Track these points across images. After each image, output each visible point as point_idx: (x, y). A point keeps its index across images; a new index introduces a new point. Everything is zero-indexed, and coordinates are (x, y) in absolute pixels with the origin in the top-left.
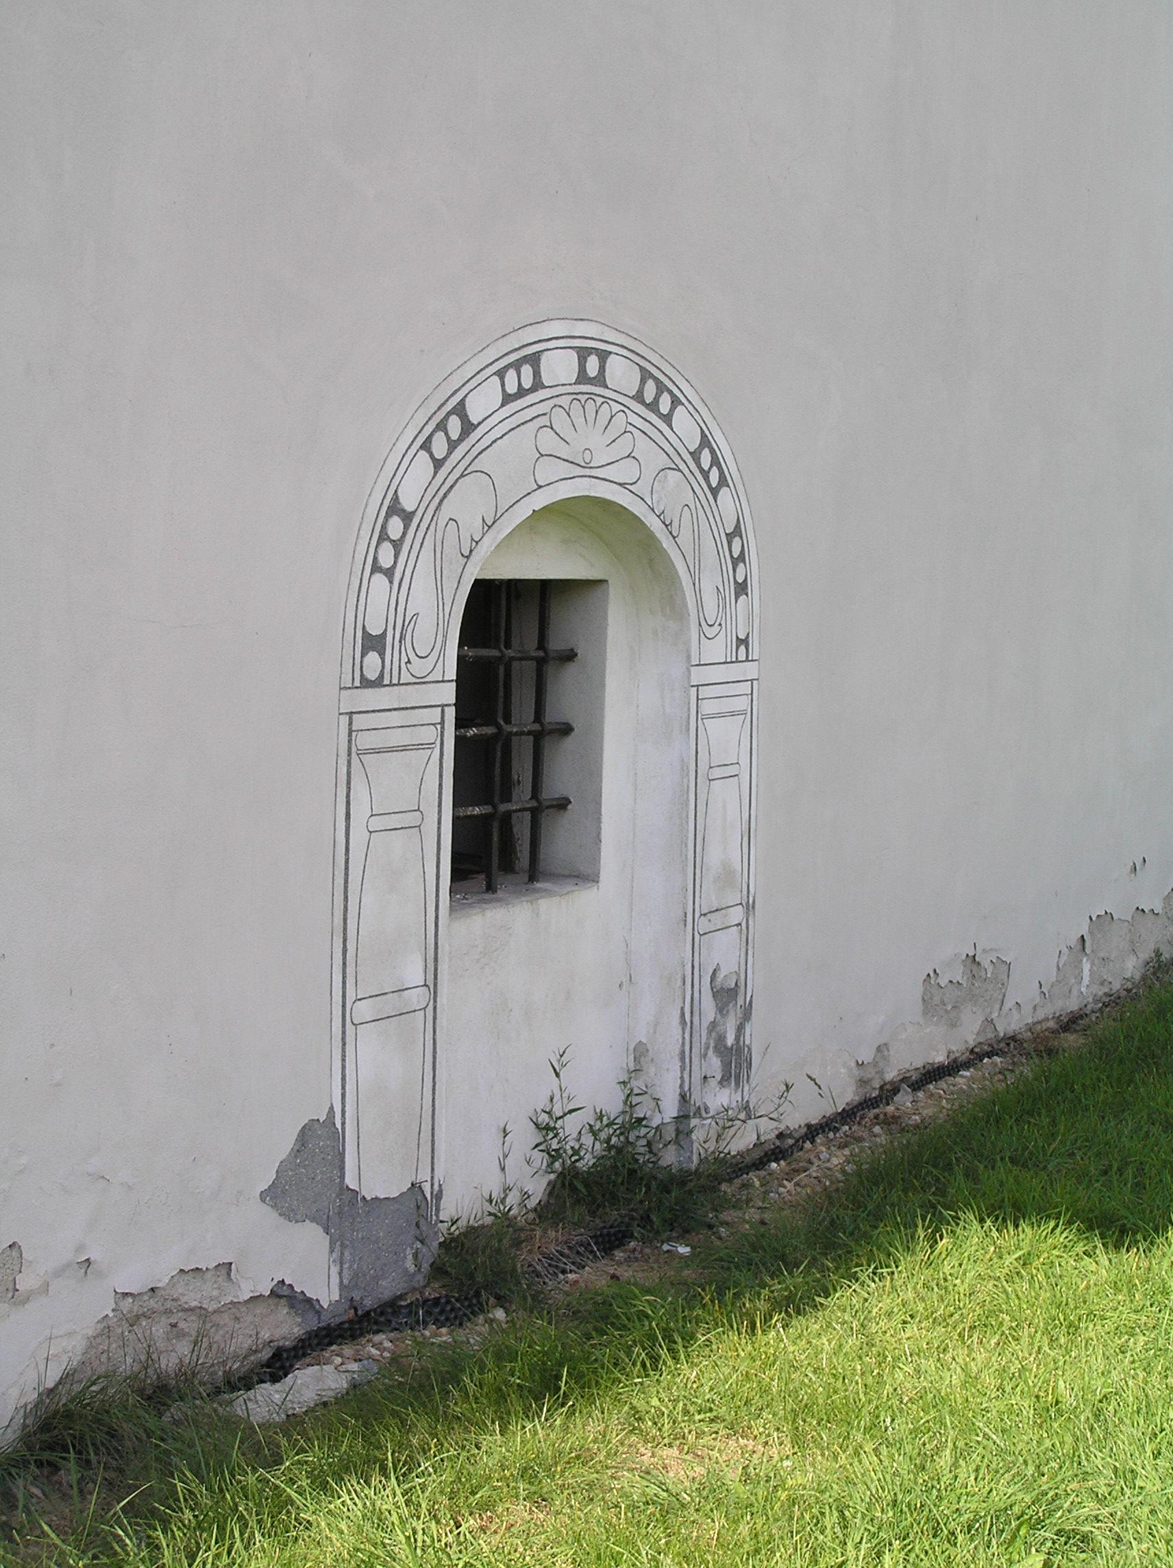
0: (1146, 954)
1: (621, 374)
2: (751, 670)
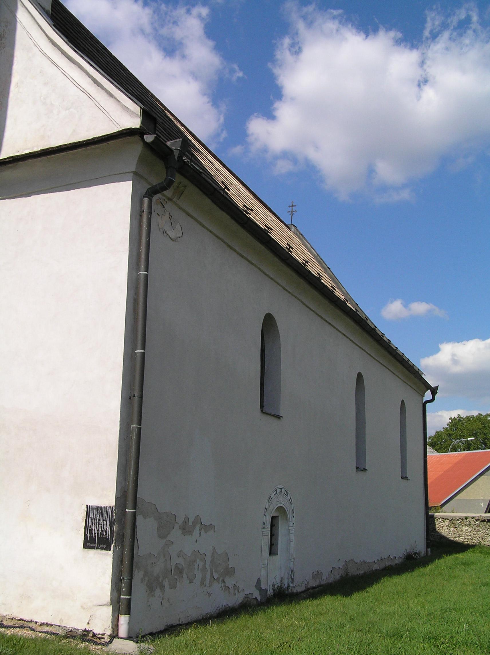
0: (340, 575)
1: (283, 491)
2: (294, 527)
